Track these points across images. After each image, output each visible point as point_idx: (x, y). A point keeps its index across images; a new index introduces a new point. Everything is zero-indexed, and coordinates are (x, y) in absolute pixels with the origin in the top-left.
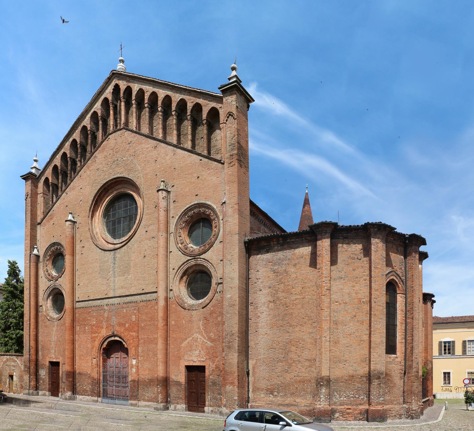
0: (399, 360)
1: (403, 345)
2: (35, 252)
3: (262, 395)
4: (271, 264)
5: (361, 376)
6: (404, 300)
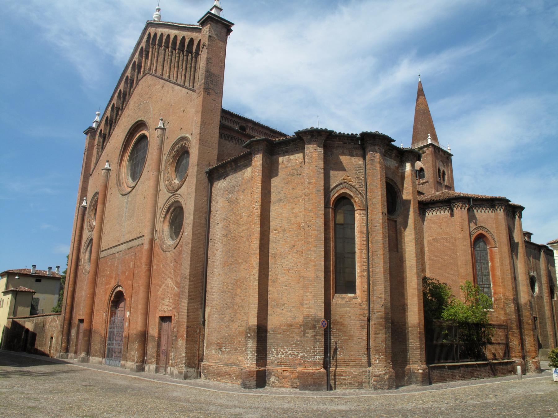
0: (359, 300)
1: (365, 280)
2: (84, 204)
3: (213, 352)
4: (226, 192)
5: (300, 325)
6: (365, 218)
